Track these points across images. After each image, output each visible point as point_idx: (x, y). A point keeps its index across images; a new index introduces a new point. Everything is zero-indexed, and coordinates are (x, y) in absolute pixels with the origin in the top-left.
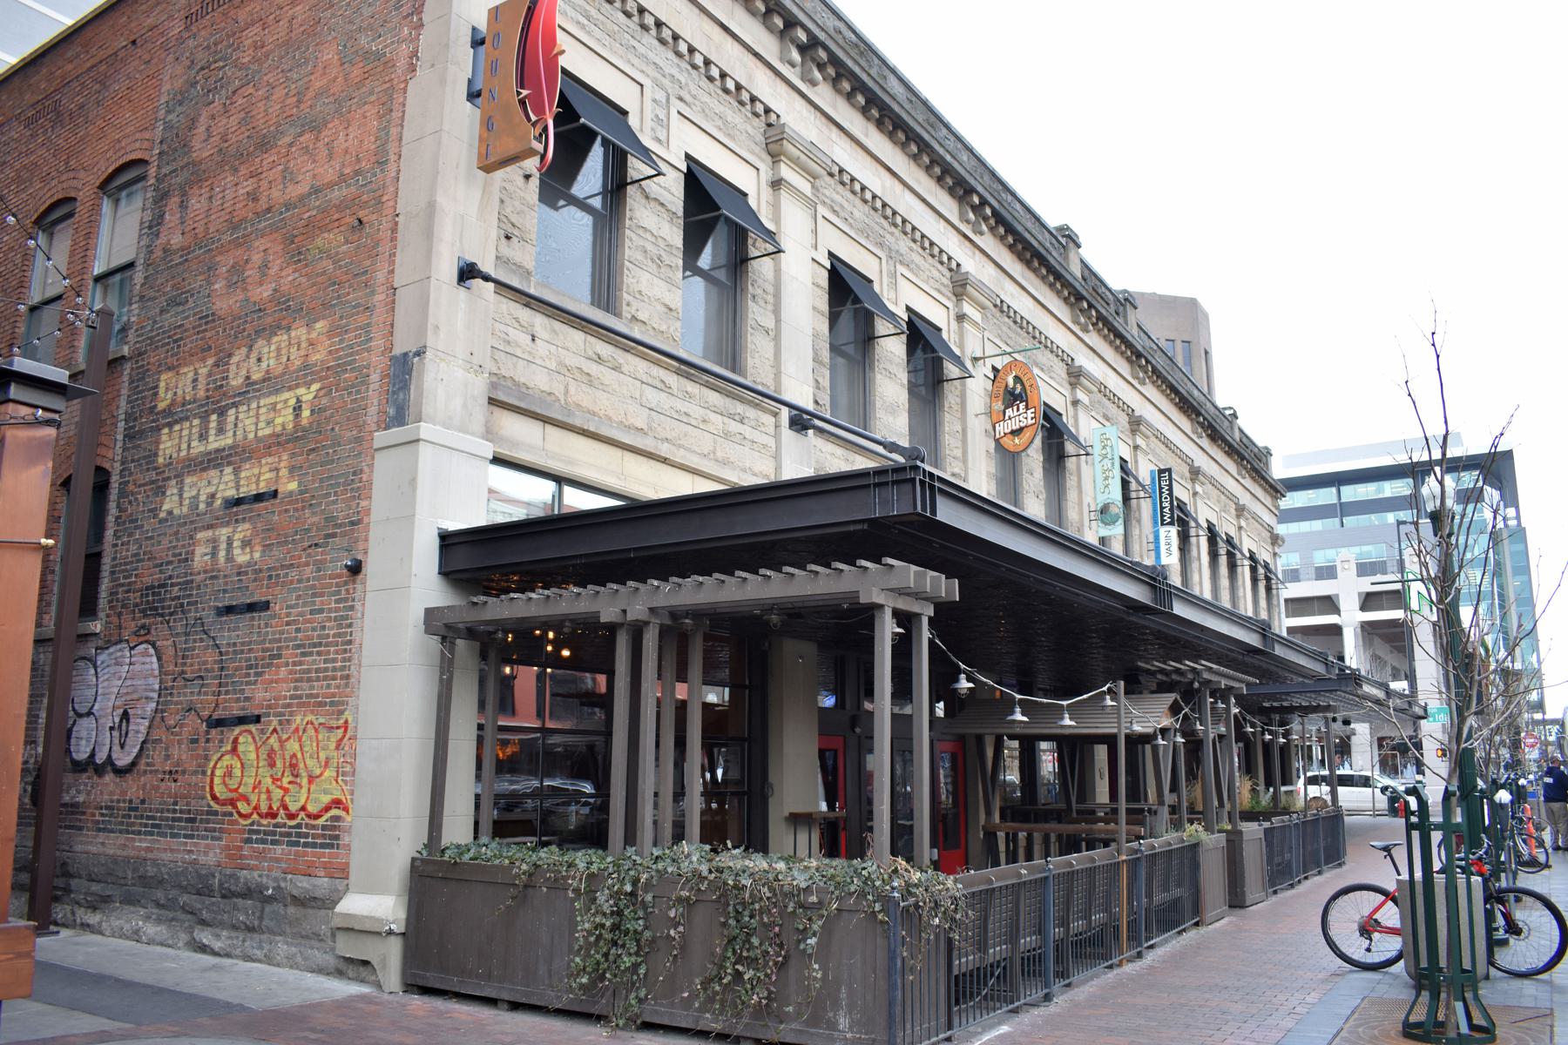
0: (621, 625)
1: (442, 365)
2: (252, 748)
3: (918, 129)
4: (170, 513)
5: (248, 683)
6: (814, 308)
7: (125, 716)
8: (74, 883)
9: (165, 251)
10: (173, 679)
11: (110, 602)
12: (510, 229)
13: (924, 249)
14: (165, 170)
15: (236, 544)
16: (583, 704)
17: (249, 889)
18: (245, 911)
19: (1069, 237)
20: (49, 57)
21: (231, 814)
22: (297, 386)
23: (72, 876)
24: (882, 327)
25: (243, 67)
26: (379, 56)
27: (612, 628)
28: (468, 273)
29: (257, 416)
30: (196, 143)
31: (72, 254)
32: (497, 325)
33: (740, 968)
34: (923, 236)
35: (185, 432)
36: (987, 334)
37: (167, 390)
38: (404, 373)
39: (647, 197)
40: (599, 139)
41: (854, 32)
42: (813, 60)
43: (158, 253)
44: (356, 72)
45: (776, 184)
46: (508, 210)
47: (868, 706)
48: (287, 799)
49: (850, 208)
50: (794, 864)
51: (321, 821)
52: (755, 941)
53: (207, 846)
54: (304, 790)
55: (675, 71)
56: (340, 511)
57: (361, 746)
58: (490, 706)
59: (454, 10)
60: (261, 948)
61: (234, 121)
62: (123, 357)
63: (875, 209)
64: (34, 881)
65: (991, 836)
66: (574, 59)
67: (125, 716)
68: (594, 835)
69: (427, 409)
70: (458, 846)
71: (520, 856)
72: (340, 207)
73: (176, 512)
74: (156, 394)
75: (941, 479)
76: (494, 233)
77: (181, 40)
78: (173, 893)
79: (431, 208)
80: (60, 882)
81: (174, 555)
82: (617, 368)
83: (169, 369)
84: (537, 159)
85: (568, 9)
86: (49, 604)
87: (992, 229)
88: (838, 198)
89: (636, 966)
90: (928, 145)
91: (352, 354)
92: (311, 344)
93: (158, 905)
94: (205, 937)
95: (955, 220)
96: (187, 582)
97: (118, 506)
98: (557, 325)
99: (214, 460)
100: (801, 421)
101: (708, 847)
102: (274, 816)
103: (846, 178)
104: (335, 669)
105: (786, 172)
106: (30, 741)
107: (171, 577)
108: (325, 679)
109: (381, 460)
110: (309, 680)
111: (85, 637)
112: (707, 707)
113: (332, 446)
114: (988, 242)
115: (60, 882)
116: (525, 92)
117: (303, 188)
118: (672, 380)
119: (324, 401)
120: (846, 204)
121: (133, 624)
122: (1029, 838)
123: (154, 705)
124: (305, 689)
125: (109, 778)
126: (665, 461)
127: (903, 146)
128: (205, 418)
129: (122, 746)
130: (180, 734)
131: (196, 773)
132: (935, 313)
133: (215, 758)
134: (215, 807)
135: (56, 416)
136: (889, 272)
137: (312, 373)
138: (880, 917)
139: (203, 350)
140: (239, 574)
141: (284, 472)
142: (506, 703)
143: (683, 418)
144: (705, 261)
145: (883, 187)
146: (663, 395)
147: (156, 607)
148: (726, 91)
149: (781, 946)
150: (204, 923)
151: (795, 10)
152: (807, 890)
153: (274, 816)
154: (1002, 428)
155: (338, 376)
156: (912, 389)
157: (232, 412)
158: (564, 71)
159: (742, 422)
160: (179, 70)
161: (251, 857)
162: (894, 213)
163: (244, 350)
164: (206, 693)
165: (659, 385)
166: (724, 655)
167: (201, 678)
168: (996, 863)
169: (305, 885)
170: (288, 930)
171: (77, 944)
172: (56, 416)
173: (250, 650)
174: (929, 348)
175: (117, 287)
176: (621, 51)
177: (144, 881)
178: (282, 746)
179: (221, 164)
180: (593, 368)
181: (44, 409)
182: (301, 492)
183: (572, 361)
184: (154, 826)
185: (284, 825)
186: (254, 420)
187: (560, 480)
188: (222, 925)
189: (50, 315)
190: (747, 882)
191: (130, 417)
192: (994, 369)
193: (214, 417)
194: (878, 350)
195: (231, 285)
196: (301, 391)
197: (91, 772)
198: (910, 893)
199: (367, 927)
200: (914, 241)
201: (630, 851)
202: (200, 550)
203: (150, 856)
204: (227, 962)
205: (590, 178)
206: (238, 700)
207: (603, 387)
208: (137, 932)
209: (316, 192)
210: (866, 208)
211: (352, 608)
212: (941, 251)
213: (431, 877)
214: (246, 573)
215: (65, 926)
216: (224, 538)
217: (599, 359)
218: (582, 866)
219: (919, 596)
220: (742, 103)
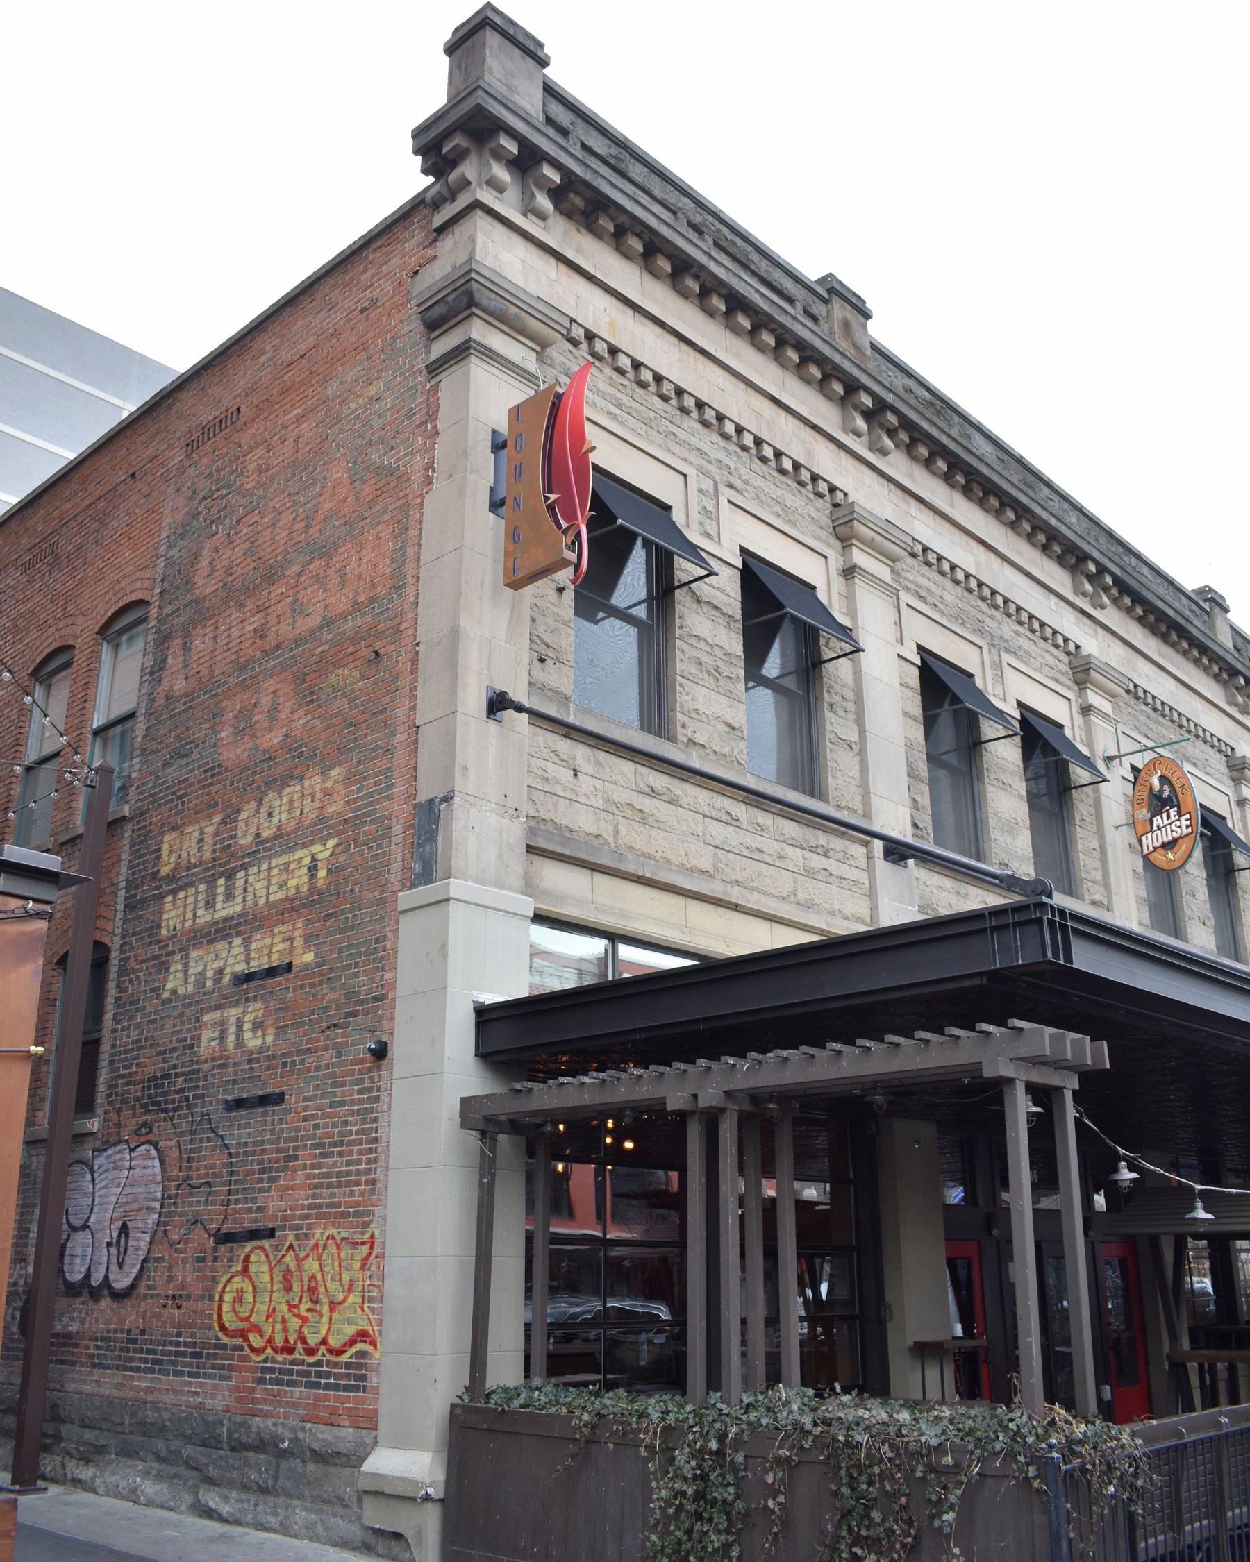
0: (692, 1113)
1: (473, 810)
2: (265, 1268)
3: (1014, 492)
4: (174, 992)
5: (261, 1190)
6: (905, 713)
7: (124, 1230)
8: (65, 1429)
9: (168, 698)
10: (179, 1185)
11: (109, 1096)
12: (543, 650)
13: (1033, 631)
14: (167, 611)
15: (246, 1026)
16: (652, 1206)
17: (262, 1440)
18: (257, 1467)
19: (1212, 600)
20: (45, 498)
21: (242, 1348)
22: (312, 842)
23: (63, 1421)
24: (989, 729)
25: (249, 493)
26: (391, 470)
27: (683, 1116)
28: (498, 704)
29: (269, 878)
30: (200, 580)
31: (70, 707)
32: (534, 761)
33: (859, 1551)
34: (1031, 617)
35: (191, 900)
36: (1120, 727)
37: (171, 852)
38: (430, 822)
39: (699, 601)
40: (639, 543)
41: (928, 389)
42: (882, 426)
43: (161, 701)
44: (368, 490)
45: (849, 572)
46: (541, 629)
47: (1004, 1196)
48: (305, 1330)
49: (938, 592)
50: (921, 1415)
51: (344, 1358)
52: (876, 1516)
53: (215, 1387)
54: (325, 1319)
55: (722, 456)
56: (362, 986)
57: (390, 1266)
58: (539, 1207)
59: (471, 413)
60: (276, 1514)
61: (239, 552)
62: (124, 818)
63: (970, 591)
64: (21, 1427)
65: (1179, 1368)
66: (607, 454)
67: (124, 1230)
68: (669, 1374)
69: (457, 863)
70: (506, 1390)
71: (584, 1405)
72: (353, 640)
73: (181, 991)
74: (159, 858)
75: (1076, 917)
76: (526, 656)
77: (182, 470)
78: (176, 1443)
79: (455, 634)
80: (49, 1428)
81: (179, 1041)
82: (673, 802)
83: (173, 829)
84: (571, 570)
85: (598, 400)
86: (43, 1100)
87: (1115, 601)
88: (924, 582)
89: (727, 1547)
90: (1027, 510)
91: (372, 804)
92: (327, 793)
93: (159, 1458)
94: (212, 1499)
95: (1070, 596)
96: (193, 1072)
97: (118, 986)
98: (602, 756)
99: (222, 931)
100: (897, 852)
101: (811, 1392)
102: (290, 1350)
103: (932, 558)
104: (358, 1173)
105: (859, 557)
106: (19, 1258)
107: (175, 1066)
108: (348, 1184)
109: (406, 923)
110: (330, 1186)
111: (81, 1137)
112: (803, 1207)
113: (352, 910)
114: (1111, 616)
115: (49, 1428)
116: (553, 497)
117: (314, 621)
118: (740, 810)
119: (342, 858)
120: (933, 588)
121: (133, 1122)
122: (1232, 1369)
123: (156, 1216)
124: (325, 1197)
125: (106, 1303)
126: (736, 908)
127: (998, 514)
128: (211, 883)
129: (120, 1265)
130: (185, 1251)
131: (202, 1297)
132: (1053, 707)
133: (224, 1280)
134: (224, 1339)
135: (48, 908)
136: (993, 664)
137: (328, 828)
138: (1036, 1484)
139: (210, 807)
140: (250, 1061)
141: (299, 942)
142: (560, 1203)
143: (755, 855)
144: (772, 666)
145: (978, 564)
146: (731, 829)
147: (160, 1101)
148: (783, 472)
149: (910, 1522)
150: (210, 1481)
151: (856, 373)
152: (940, 1448)
153: (290, 1350)
154: (1150, 842)
155: (357, 829)
156: (1033, 800)
157: (241, 874)
158: (597, 468)
159: (826, 856)
160: (181, 501)
161: (265, 1401)
162: (994, 593)
163: (253, 804)
164: (214, 1203)
165: (725, 818)
166: (822, 1141)
167: (208, 1184)
168: (1190, 1408)
169: (327, 1436)
170: (307, 1493)
171: (67, 1504)
172: (48, 908)
173: (263, 1151)
174: (1049, 749)
175: (118, 741)
176: (659, 439)
177: (148, 1430)
178: (299, 1266)
179: (226, 600)
180: (647, 804)
181: (35, 900)
182: (318, 965)
183: (620, 796)
184: (155, 1361)
185: (302, 1362)
186: (265, 883)
187: (614, 938)
188: (231, 1484)
189: (47, 774)
190: (863, 1438)
191: (131, 885)
192: (1134, 768)
193: (221, 881)
194: (987, 757)
195: (238, 732)
196: (317, 848)
197: (85, 1297)
198: (1073, 1452)
199: (400, 1491)
200: (1021, 623)
201: (715, 1397)
202: (207, 1035)
203: (150, 1397)
204: (237, 1530)
205: (633, 583)
206: (249, 1210)
207: (659, 825)
208: (134, 1491)
209: (328, 624)
210: (959, 590)
211: (377, 1099)
212: (1055, 632)
213: (476, 1428)
214: (258, 1060)
215: (53, 1481)
216: (233, 1020)
217: (653, 793)
218: (655, 1416)
219: (1058, 1065)
220: (802, 484)
